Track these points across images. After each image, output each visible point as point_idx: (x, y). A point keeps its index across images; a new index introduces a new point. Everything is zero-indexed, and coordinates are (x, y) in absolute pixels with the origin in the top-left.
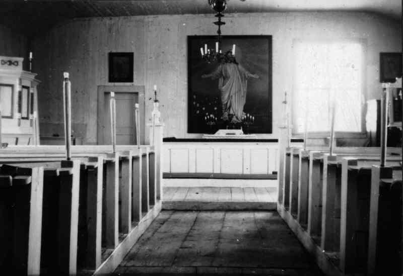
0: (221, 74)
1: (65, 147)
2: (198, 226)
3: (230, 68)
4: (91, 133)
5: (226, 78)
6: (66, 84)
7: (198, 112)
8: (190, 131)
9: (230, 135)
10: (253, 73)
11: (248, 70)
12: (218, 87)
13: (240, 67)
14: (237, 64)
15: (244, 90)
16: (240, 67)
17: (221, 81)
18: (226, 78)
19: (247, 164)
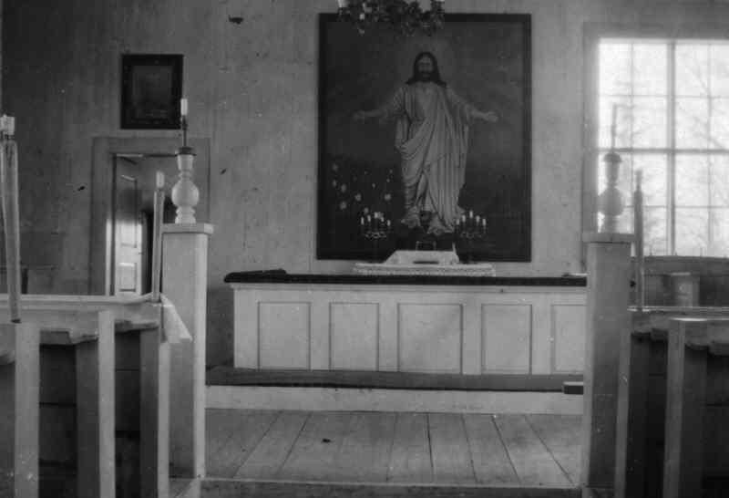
3: (426, 96)
5: (413, 119)
7: (343, 206)
13: (451, 92)
17: (401, 127)
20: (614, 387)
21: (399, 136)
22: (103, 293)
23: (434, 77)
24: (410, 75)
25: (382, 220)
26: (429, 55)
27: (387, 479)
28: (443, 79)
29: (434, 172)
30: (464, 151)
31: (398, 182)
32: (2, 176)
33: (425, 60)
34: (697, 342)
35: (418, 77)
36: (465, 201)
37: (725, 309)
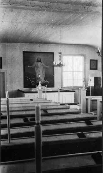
0: (36, 66)
1: (9, 115)
2: (6, 100)
3: (39, 64)
4: (33, 118)
5: (38, 67)
6: (47, 133)
7: (27, 80)
8: (25, 87)
9: (28, 102)
10: (47, 66)
11: (46, 65)
12: (35, 70)
13: (43, 63)
14: (41, 62)
15: (44, 72)
16: (43, 63)
17: (36, 68)
18: (38, 67)
19: (64, 100)
20: (89, 91)
21: (36, 70)
22: (43, 135)
23: (40, 61)
24: (37, 61)
25: (35, 126)
26: (40, 58)
27: (12, 8)
28: (42, 61)
29: (40, 75)
30: (45, 72)
31: (35, 77)
32: (1, 87)
33: (39, 59)
34: (91, 99)
35: (38, 61)
36: (45, 79)
37: (3, 143)
